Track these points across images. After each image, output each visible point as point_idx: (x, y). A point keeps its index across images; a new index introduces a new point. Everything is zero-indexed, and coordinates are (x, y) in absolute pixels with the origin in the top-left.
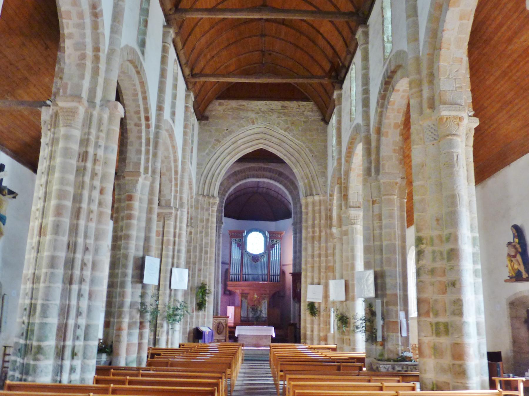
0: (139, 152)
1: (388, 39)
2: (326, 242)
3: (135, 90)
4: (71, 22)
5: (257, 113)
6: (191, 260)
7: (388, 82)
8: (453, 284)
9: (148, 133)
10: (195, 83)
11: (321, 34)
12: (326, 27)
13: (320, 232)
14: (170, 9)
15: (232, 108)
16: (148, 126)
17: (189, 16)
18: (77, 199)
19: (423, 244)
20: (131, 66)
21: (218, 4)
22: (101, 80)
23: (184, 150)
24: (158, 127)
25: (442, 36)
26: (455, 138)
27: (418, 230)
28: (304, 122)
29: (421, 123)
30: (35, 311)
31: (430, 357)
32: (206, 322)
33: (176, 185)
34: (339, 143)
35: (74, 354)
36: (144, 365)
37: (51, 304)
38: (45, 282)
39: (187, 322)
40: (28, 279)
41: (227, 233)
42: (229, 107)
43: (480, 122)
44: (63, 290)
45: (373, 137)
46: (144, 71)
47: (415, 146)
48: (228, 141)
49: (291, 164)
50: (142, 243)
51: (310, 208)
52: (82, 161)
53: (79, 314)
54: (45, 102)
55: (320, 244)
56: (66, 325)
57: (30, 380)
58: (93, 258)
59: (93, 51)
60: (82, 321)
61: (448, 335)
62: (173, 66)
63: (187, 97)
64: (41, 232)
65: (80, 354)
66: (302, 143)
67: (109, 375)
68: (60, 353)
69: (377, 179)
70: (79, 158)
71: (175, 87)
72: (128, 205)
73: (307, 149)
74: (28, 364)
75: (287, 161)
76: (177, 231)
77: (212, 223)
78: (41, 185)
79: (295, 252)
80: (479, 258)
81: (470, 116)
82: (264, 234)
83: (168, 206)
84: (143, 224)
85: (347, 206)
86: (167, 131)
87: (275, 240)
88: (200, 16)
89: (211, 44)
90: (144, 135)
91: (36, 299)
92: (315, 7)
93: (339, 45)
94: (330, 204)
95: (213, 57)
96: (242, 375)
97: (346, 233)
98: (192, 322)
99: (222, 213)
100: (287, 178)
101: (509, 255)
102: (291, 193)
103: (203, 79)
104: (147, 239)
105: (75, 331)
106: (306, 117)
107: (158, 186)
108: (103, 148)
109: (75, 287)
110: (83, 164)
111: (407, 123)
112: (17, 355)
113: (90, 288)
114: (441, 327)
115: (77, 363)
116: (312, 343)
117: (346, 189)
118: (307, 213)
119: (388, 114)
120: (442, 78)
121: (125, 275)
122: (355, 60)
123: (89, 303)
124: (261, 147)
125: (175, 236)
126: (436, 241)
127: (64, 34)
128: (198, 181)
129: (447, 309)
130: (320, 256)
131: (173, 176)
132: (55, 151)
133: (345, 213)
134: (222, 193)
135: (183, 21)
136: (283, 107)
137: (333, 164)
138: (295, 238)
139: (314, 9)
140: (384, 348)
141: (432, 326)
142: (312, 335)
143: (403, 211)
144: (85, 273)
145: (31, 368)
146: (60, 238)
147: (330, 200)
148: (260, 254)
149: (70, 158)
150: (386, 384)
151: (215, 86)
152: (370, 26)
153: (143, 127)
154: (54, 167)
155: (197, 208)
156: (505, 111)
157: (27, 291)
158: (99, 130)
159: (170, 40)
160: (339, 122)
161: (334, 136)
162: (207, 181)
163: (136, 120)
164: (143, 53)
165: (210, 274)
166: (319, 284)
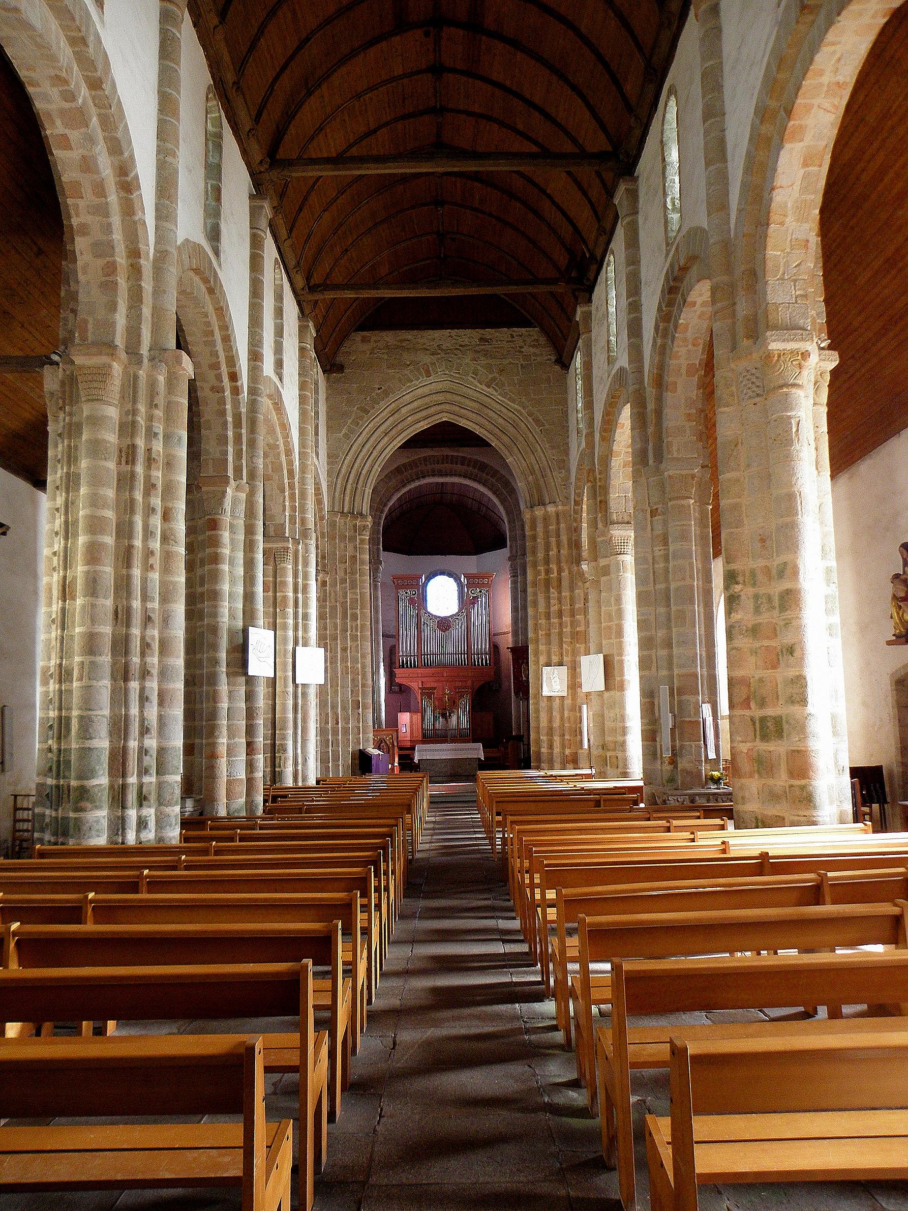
0: (223, 440)
1: (674, 204)
2: (572, 590)
3: (208, 324)
4: (82, 203)
7: (674, 290)
8: (791, 650)
9: (236, 404)
10: (316, 302)
11: (549, 197)
12: (557, 181)
13: (560, 570)
14: (261, 162)
15: (387, 347)
16: (236, 391)
17: (297, 173)
18: (124, 531)
19: (737, 583)
20: (196, 279)
21: (351, 146)
22: (146, 311)
23: (302, 432)
24: (253, 391)
25: (771, 200)
26: (794, 390)
27: (728, 561)
29: (732, 366)
30: (68, 730)
31: (751, 776)
33: (292, 496)
34: (589, 405)
35: (142, 799)
36: (260, 812)
37: (96, 715)
38: (80, 679)
40: (51, 676)
41: (389, 580)
42: (381, 344)
43: (840, 361)
44: (113, 691)
45: (650, 392)
46: (221, 286)
47: (723, 409)
48: (384, 408)
49: (502, 447)
51: (540, 529)
52: (127, 463)
53: (144, 730)
54: (49, 358)
55: (560, 593)
56: (125, 749)
57: (72, 843)
58: (160, 633)
59: (128, 257)
60: (151, 743)
61: (782, 737)
62: (273, 274)
63: (302, 330)
64: (66, 591)
65: (153, 798)
67: (203, 829)
68: (118, 797)
69: (658, 471)
70: (120, 457)
71: (279, 312)
72: (210, 537)
73: (530, 419)
74: (65, 819)
78: (57, 510)
79: (515, 609)
80: (837, 604)
81: (823, 349)
82: (457, 580)
83: (281, 537)
84: (240, 571)
85: (608, 522)
86: (270, 397)
88: (320, 174)
89: (341, 225)
91: (69, 709)
92: (535, 143)
93: (583, 215)
94: (575, 520)
95: (346, 250)
96: (431, 826)
97: (606, 571)
99: (378, 544)
100: (495, 473)
101: (894, 597)
102: (503, 502)
103: (330, 295)
104: (249, 597)
105: (140, 760)
106: (527, 357)
107: (261, 500)
108: (161, 437)
109: (134, 685)
110: (129, 467)
111: (709, 365)
112: (44, 806)
113: (159, 685)
114: (769, 724)
115: (150, 812)
117: (605, 489)
118: (534, 538)
119: (676, 349)
120: (771, 280)
121: (215, 662)
122: (612, 245)
123: (159, 711)
125: (296, 591)
126: (760, 577)
127: (71, 226)
128: (332, 487)
129: (780, 693)
130: (560, 614)
132: (76, 448)
133: (603, 534)
134: (377, 506)
135: (286, 185)
136: (481, 339)
137: (579, 446)
138: (514, 583)
139: (534, 149)
140: (676, 767)
141: (754, 724)
143: (707, 527)
144: (148, 659)
145: (71, 824)
146: (101, 601)
147: (576, 512)
148: (452, 616)
149: (105, 459)
150: (675, 823)
151: (354, 304)
152: (640, 179)
153: (227, 393)
154: (78, 476)
156: (891, 334)
157: (51, 695)
158: (152, 405)
159: (264, 223)
160: (588, 365)
161: (579, 391)
162: (349, 487)
163: (213, 382)
164: (217, 253)
165: (363, 656)
166: (561, 664)
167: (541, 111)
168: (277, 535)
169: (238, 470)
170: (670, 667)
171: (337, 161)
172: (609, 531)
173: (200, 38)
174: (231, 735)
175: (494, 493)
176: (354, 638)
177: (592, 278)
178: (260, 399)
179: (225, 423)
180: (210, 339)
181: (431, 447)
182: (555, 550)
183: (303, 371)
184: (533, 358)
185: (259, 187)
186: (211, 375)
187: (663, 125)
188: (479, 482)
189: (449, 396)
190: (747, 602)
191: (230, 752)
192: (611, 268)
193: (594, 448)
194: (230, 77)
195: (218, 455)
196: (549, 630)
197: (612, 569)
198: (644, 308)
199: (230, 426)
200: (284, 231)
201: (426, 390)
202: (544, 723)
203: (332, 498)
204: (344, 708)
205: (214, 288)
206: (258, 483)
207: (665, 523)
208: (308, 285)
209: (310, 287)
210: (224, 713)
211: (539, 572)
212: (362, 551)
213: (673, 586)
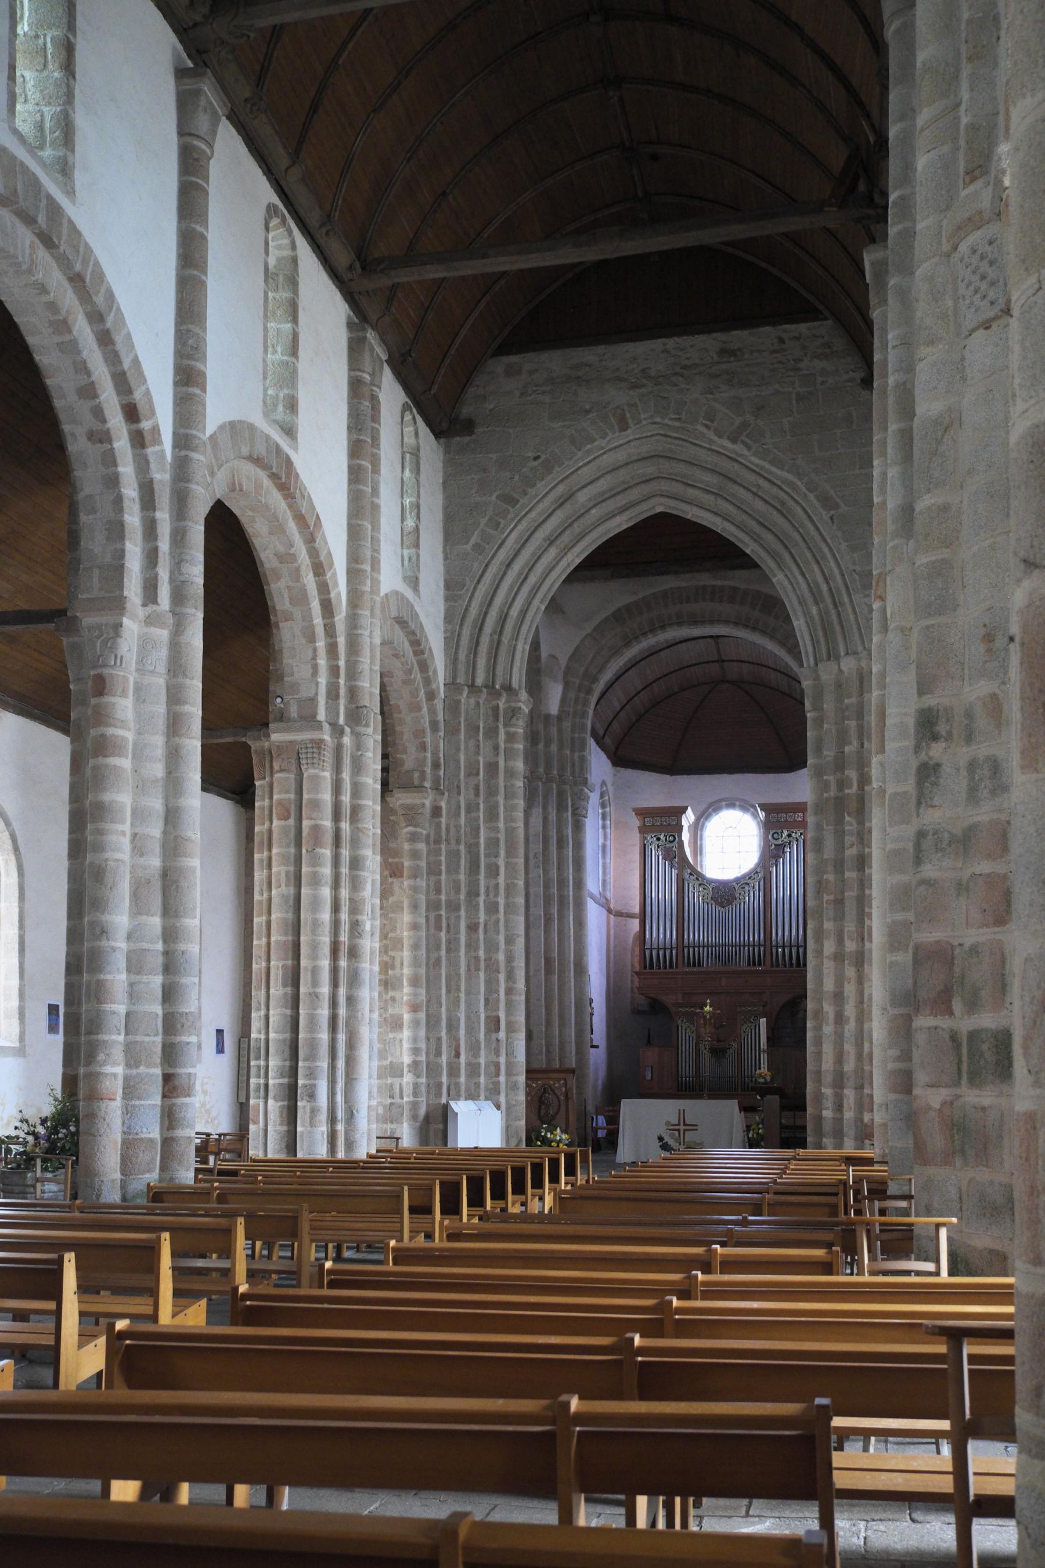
5: (634, 387)
6: (443, 897)
9: (142, 465)
32: (503, 1087)
33: (332, 649)
39: (439, 1085)
50: (155, 830)
51: (829, 705)
66: (790, 477)
75: (750, 548)
76: (346, 799)
77: (510, 774)
87: (785, 833)
90: (127, 470)
95: (444, 194)
98: (457, 1084)
114: (985, 1047)
116: (839, 1146)
124: (659, 506)
125: (337, 816)
131: (318, 621)
136: (722, 352)
142: (838, 1121)
148: (737, 880)
153: (122, 444)
155: (452, 731)
163: (89, 422)
165: (510, 940)
168: (302, 718)
174: (133, 1056)
178: (194, 456)
179: (119, 501)
180: (67, 338)
181: (676, 573)
182: (855, 743)
184: (820, 379)
188: (763, 632)
190: (954, 781)
191: (130, 1090)
195: (108, 559)
196: (842, 892)
201: (621, 456)
202: (828, 1064)
203: (453, 660)
204: (471, 1030)
206: (190, 611)
212: (509, 754)
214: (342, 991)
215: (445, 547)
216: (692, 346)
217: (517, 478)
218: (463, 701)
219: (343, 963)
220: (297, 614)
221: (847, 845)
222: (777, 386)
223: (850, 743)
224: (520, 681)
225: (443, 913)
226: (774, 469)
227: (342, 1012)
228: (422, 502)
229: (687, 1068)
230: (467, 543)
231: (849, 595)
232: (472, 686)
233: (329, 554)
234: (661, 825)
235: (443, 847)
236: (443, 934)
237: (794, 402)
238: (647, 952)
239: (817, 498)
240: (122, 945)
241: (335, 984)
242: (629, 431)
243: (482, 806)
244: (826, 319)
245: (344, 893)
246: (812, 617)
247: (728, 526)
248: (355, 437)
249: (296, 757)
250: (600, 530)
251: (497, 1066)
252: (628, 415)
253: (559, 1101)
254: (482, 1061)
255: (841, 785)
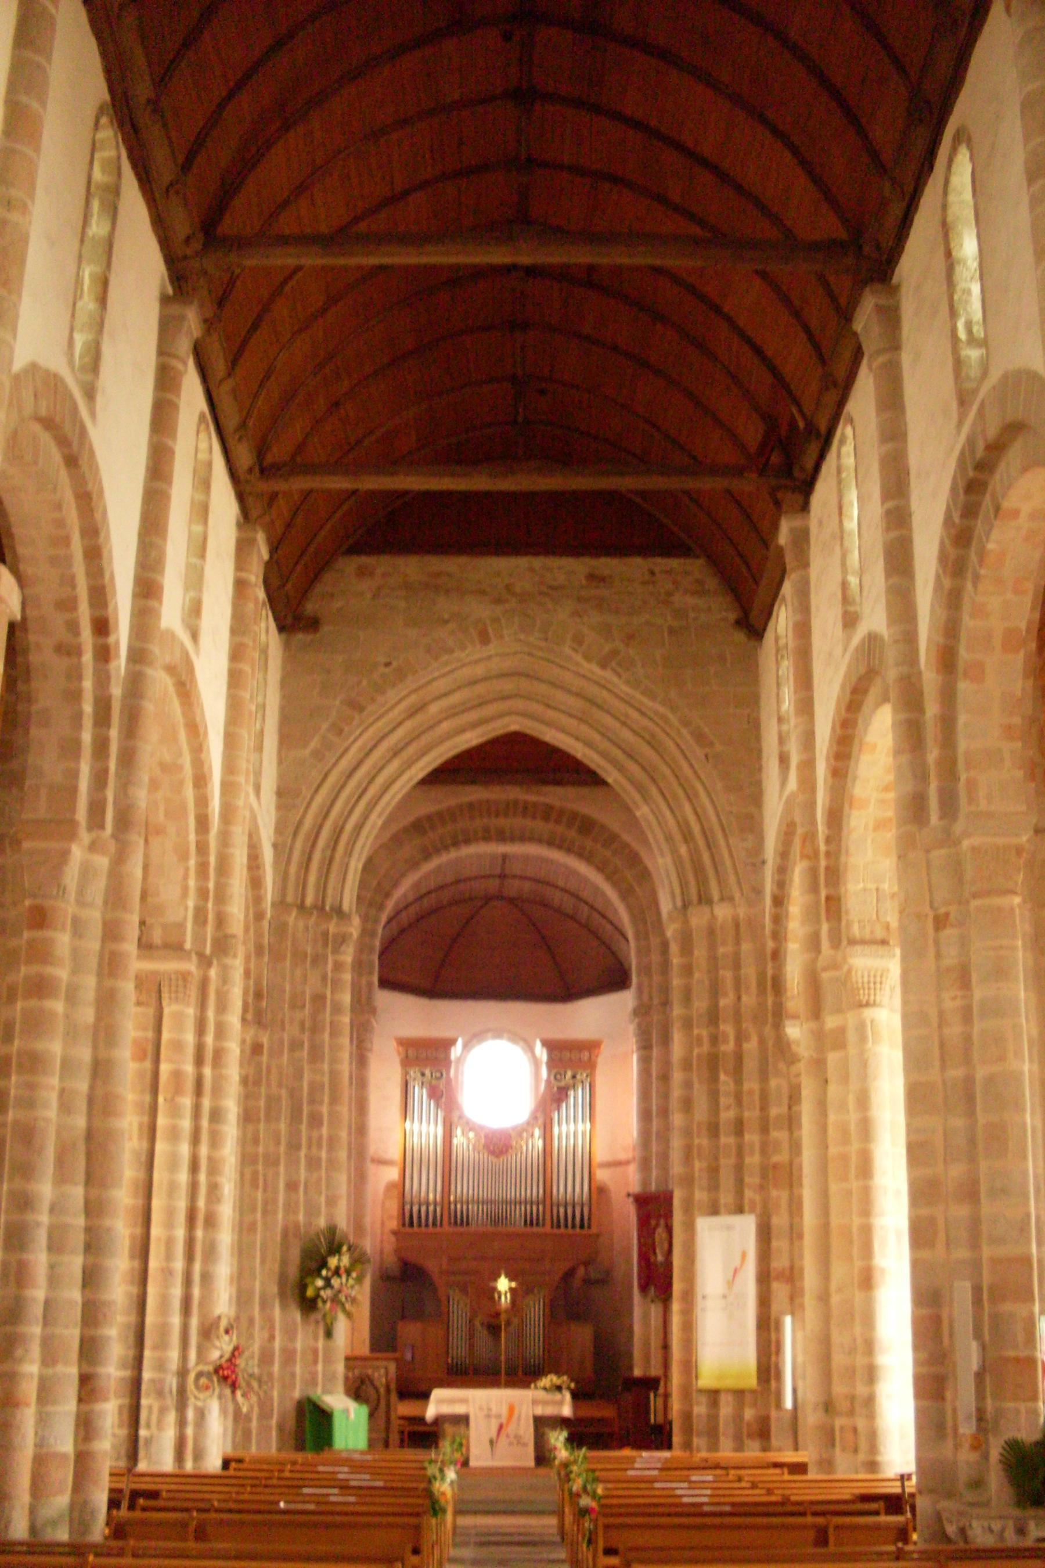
0: (71, 749)
3: (60, 523)
5: (498, 601)
9: (102, 680)
10: (273, 497)
11: (730, 320)
14: (188, 239)
15: (407, 586)
16: (104, 654)
17: (253, 260)
20: (46, 438)
21: (357, 219)
23: (230, 741)
24: (138, 656)
28: (671, 631)
45: (930, 678)
48: (396, 700)
55: (738, 1082)
62: (195, 442)
63: (243, 547)
66: (662, 710)
71: (202, 511)
77: (337, 1009)
86: (171, 669)
87: (569, 1074)
92: (702, 223)
95: (337, 404)
100: (611, 839)
103: (300, 484)
107: (139, 873)
116: (714, 1446)
117: (835, 875)
118: (688, 970)
124: (514, 724)
125: (199, 1061)
130: (739, 1127)
134: (375, 887)
135: (232, 281)
136: (592, 577)
138: (645, 1061)
152: (904, 290)
153: (88, 657)
159: (184, 346)
160: (803, 630)
162: (317, 856)
163: (62, 634)
167: (713, 168)
169: (97, 809)
170: (975, 1244)
171: (328, 241)
172: (845, 959)
173: (93, 23)
174: (49, 1358)
175: (608, 878)
176: (313, 1163)
177: (809, 465)
182: (732, 996)
183: (239, 625)
184: (692, 615)
185: (181, 278)
186: (58, 621)
187: (945, 193)
189: (524, 684)
191: (46, 1392)
192: (848, 449)
193: (813, 790)
194: (143, 90)
197: (851, 1036)
198: (917, 521)
199: (88, 723)
200: (222, 361)
201: (479, 670)
203: (283, 878)
205: (76, 456)
207: (964, 943)
208: (260, 465)
209: (260, 473)
210: (37, 1310)
211: (699, 1039)
213: (980, 1073)
214: (197, 1267)
215: (280, 751)
216: (559, 568)
217: (365, 683)
218: (291, 924)
219: (199, 1233)
220: (171, 829)
221: (722, 1107)
222: (647, 616)
223: (726, 994)
224: (351, 903)
225: (260, 1168)
226: (645, 700)
227: (196, 1292)
228: (267, 702)
229: (459, 1349)
230: (305, 746)
231: (725, 836)
232: (302, 907)
233: (210, 767)
234: (428, 1057)
235: (263, 1090)
236: (259, 1195)
237: (666, 634)
238: (407, 1207)
239: (692, 734)
240: (44, 1218)
241: (190, 1257)
242: (491, 646)
243: (306, 1044)
244: (698, 557)
245: (204, 1150)
246: (680, 857)
247: (588, 751)
248: (237, 639)
249: (156, 988)
250: (449, 744)
251: (315, 1352)
252: (490, 630)
253: (379, 1396)
254: (299, 1345)
255: (715, 1040)
